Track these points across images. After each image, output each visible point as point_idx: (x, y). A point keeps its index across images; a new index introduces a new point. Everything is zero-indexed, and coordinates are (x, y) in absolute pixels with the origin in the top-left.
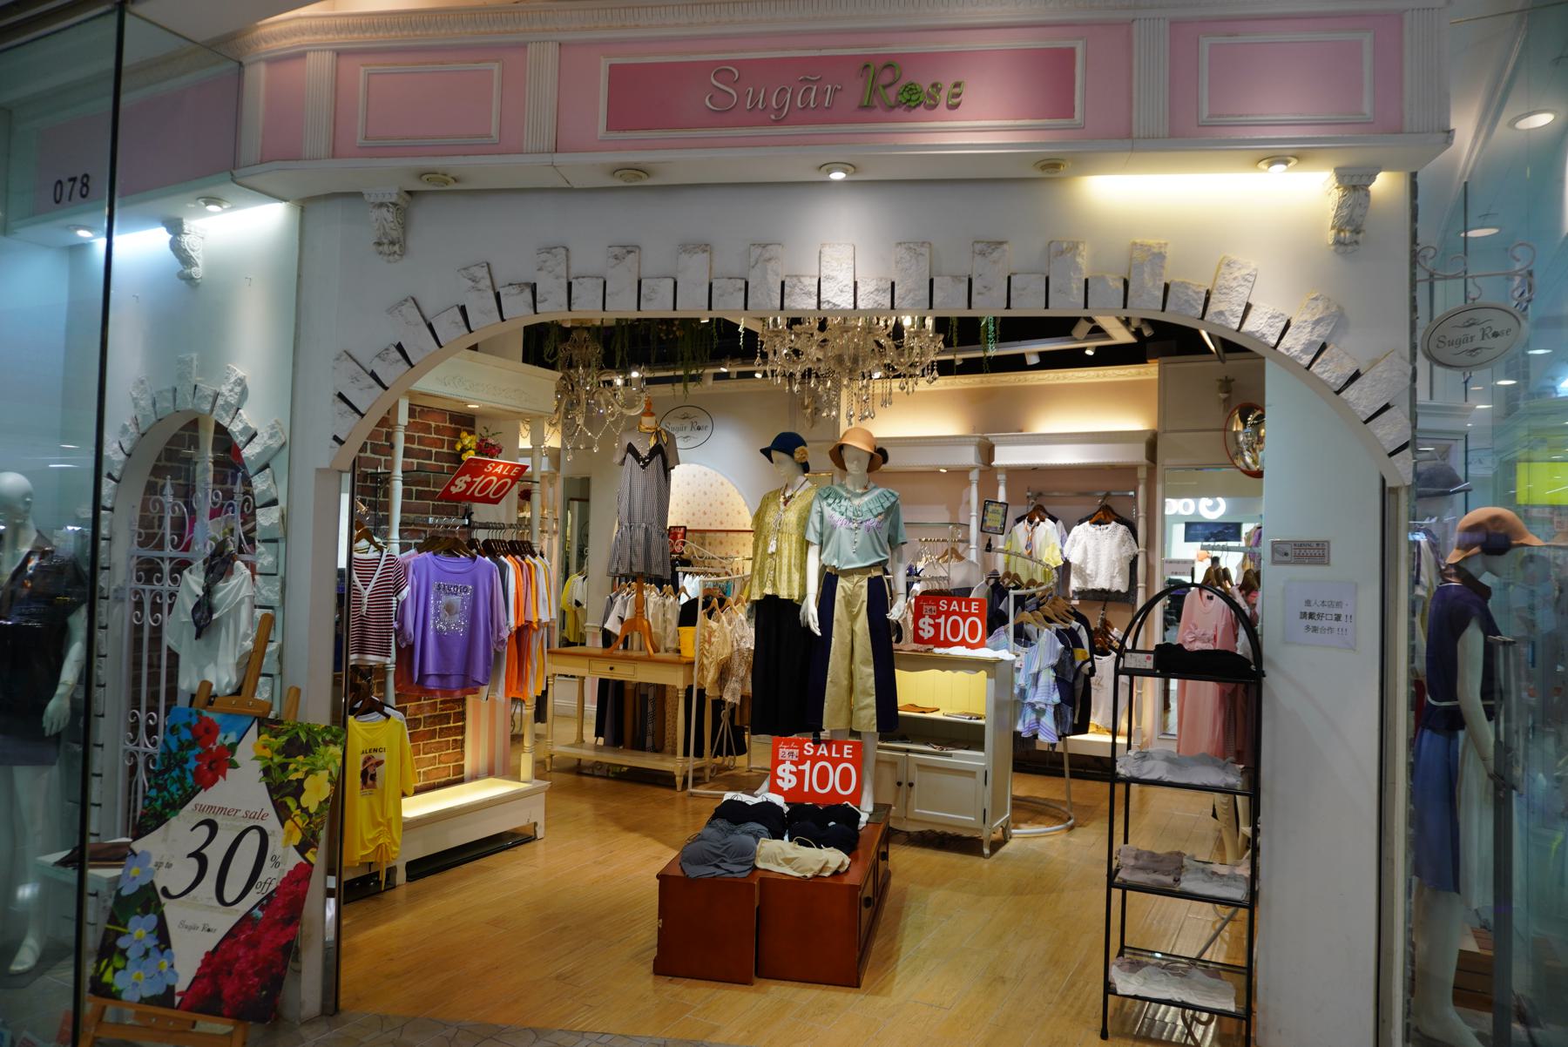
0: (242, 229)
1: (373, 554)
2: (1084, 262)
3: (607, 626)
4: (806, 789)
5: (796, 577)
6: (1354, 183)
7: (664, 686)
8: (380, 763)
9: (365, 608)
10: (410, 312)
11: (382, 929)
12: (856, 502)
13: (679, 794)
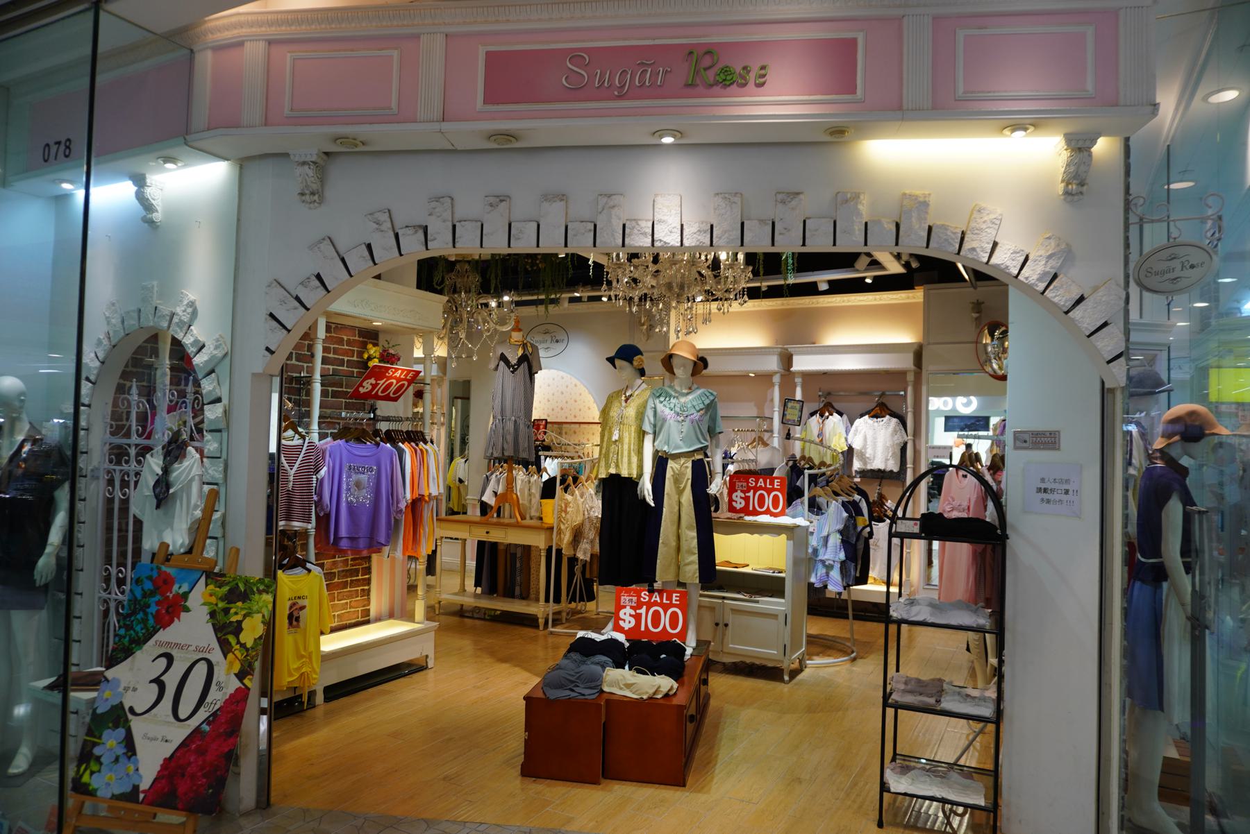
0: (193, 182)
1: (297, 441)
2: (865, 209)
3: (484, 499)
4: (643, 628)
5: (635, 459)
6: (1080, 146)
7: (530, 547)
8: (303, 608)
9: (291, 484)
10: (327, 248)
11: (304, 740)
12: (683, 400)
13: (541, 633)
